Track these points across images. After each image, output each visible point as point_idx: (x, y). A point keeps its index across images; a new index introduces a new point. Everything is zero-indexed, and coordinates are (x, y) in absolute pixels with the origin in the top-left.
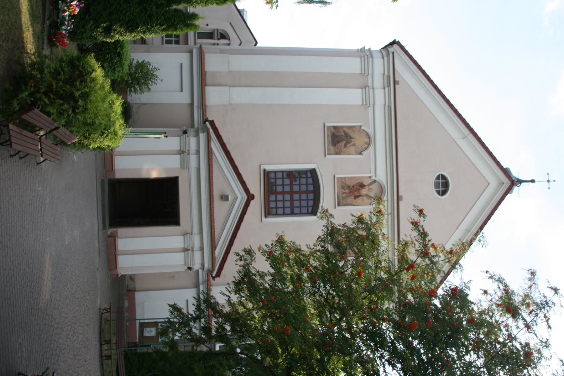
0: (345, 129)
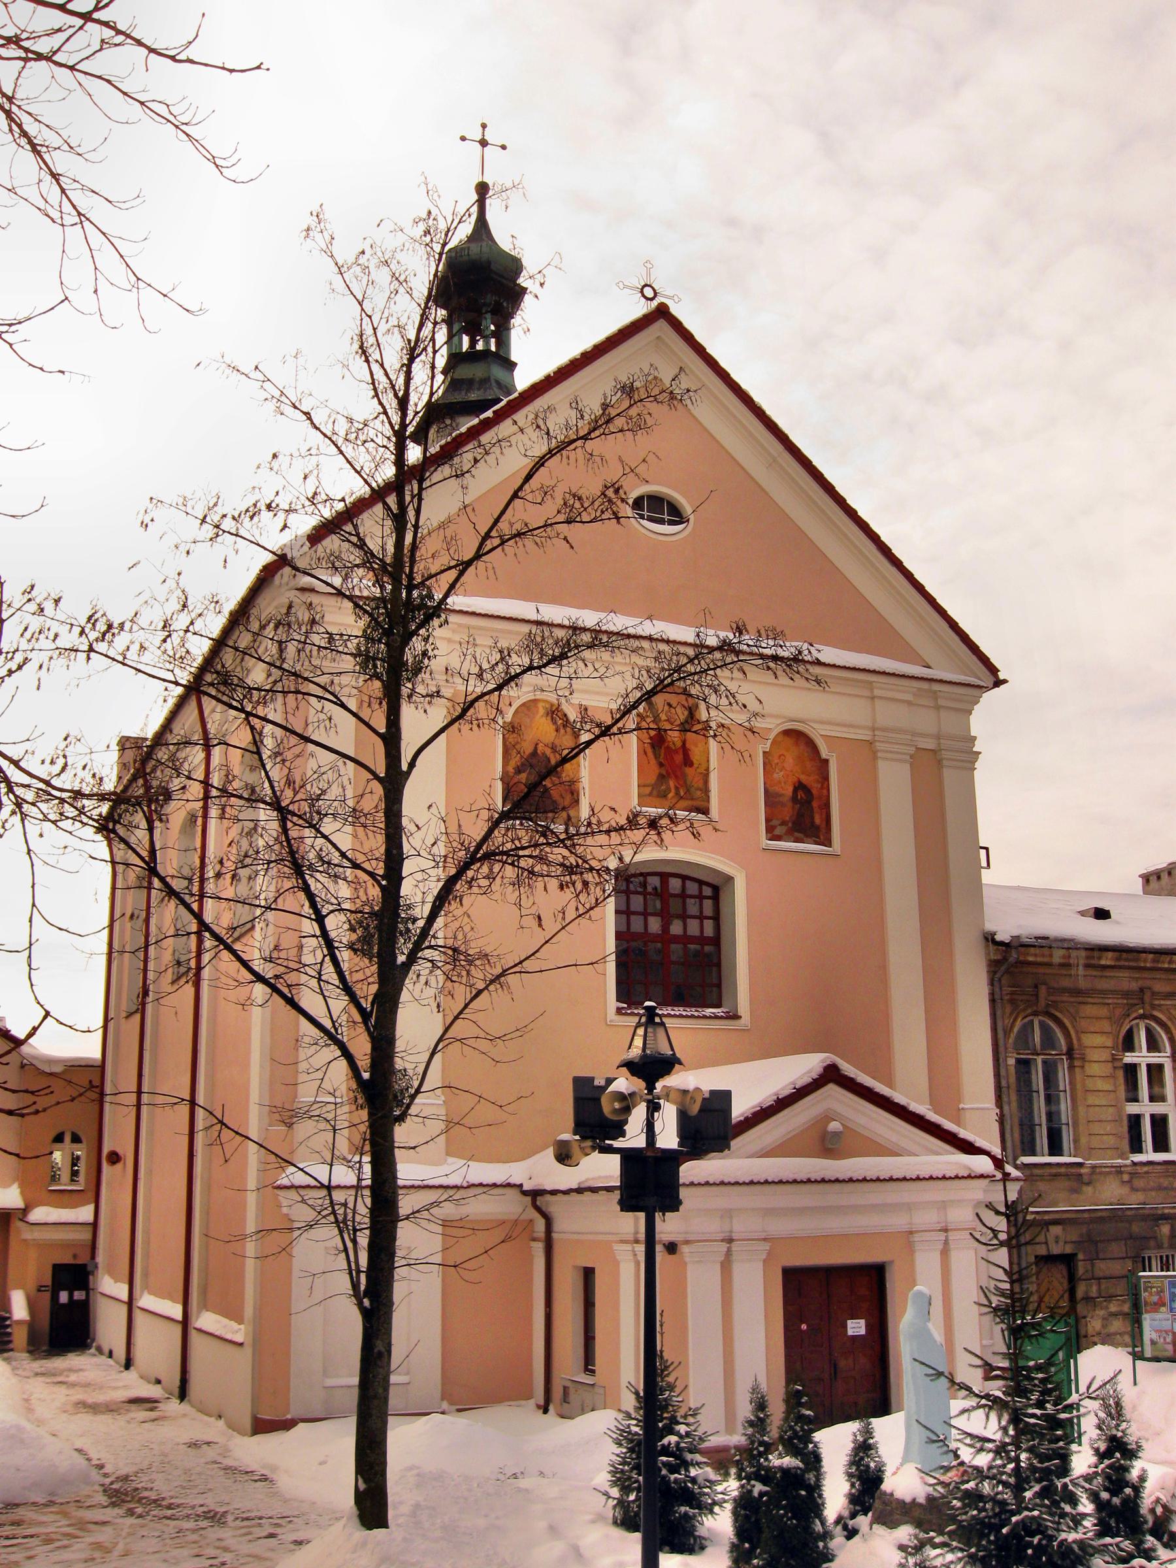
0: (510, 769)
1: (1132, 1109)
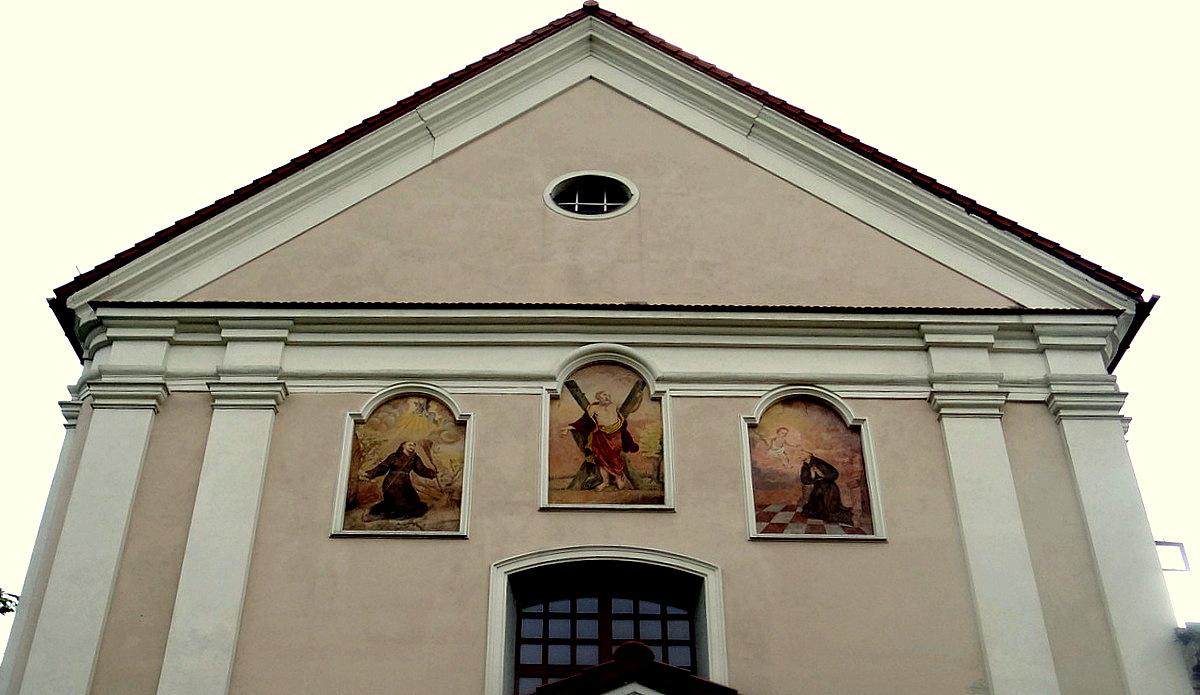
0: (362, 473)
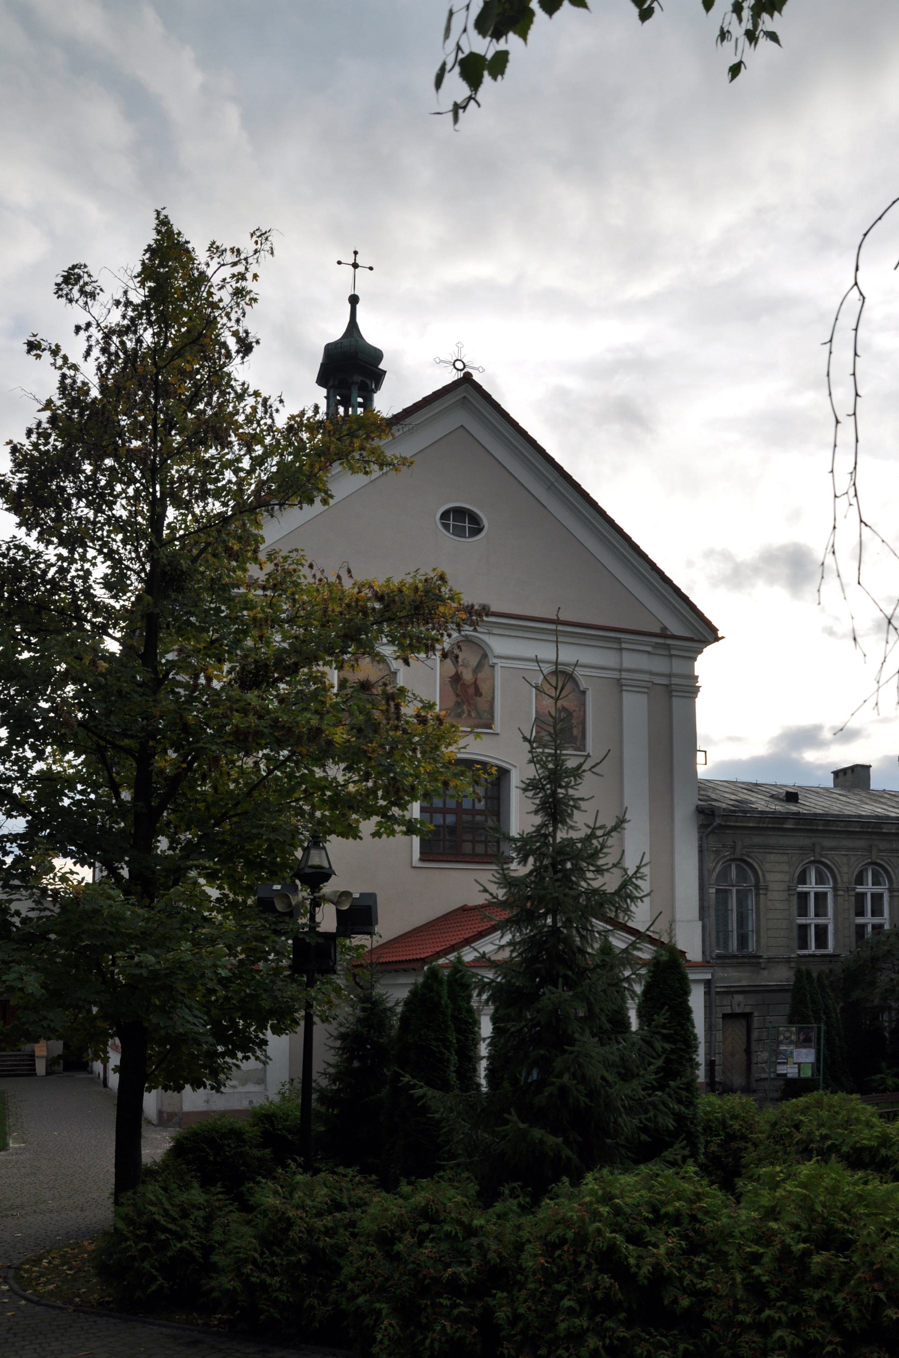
1: (860, 920)
